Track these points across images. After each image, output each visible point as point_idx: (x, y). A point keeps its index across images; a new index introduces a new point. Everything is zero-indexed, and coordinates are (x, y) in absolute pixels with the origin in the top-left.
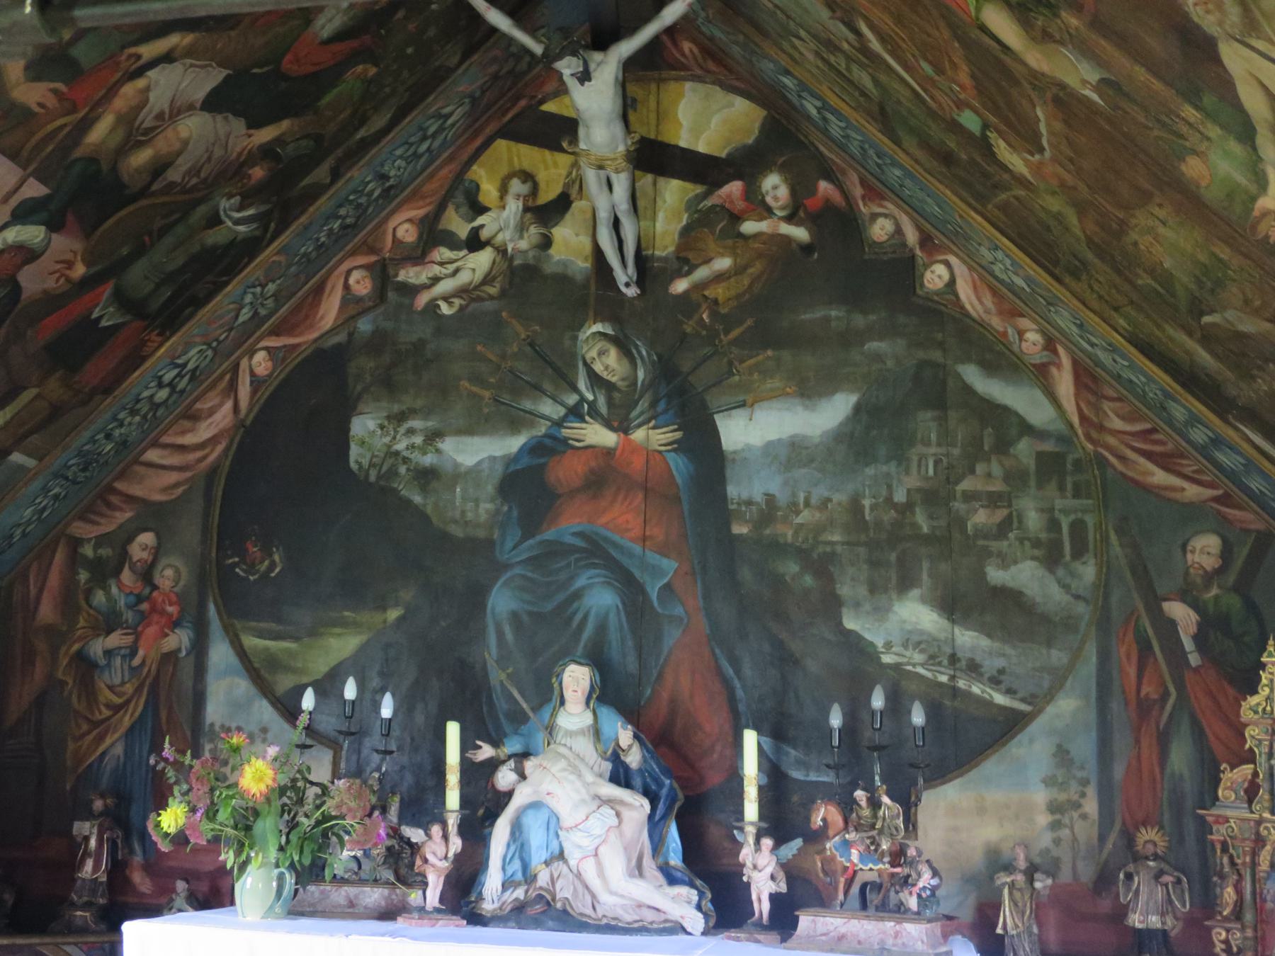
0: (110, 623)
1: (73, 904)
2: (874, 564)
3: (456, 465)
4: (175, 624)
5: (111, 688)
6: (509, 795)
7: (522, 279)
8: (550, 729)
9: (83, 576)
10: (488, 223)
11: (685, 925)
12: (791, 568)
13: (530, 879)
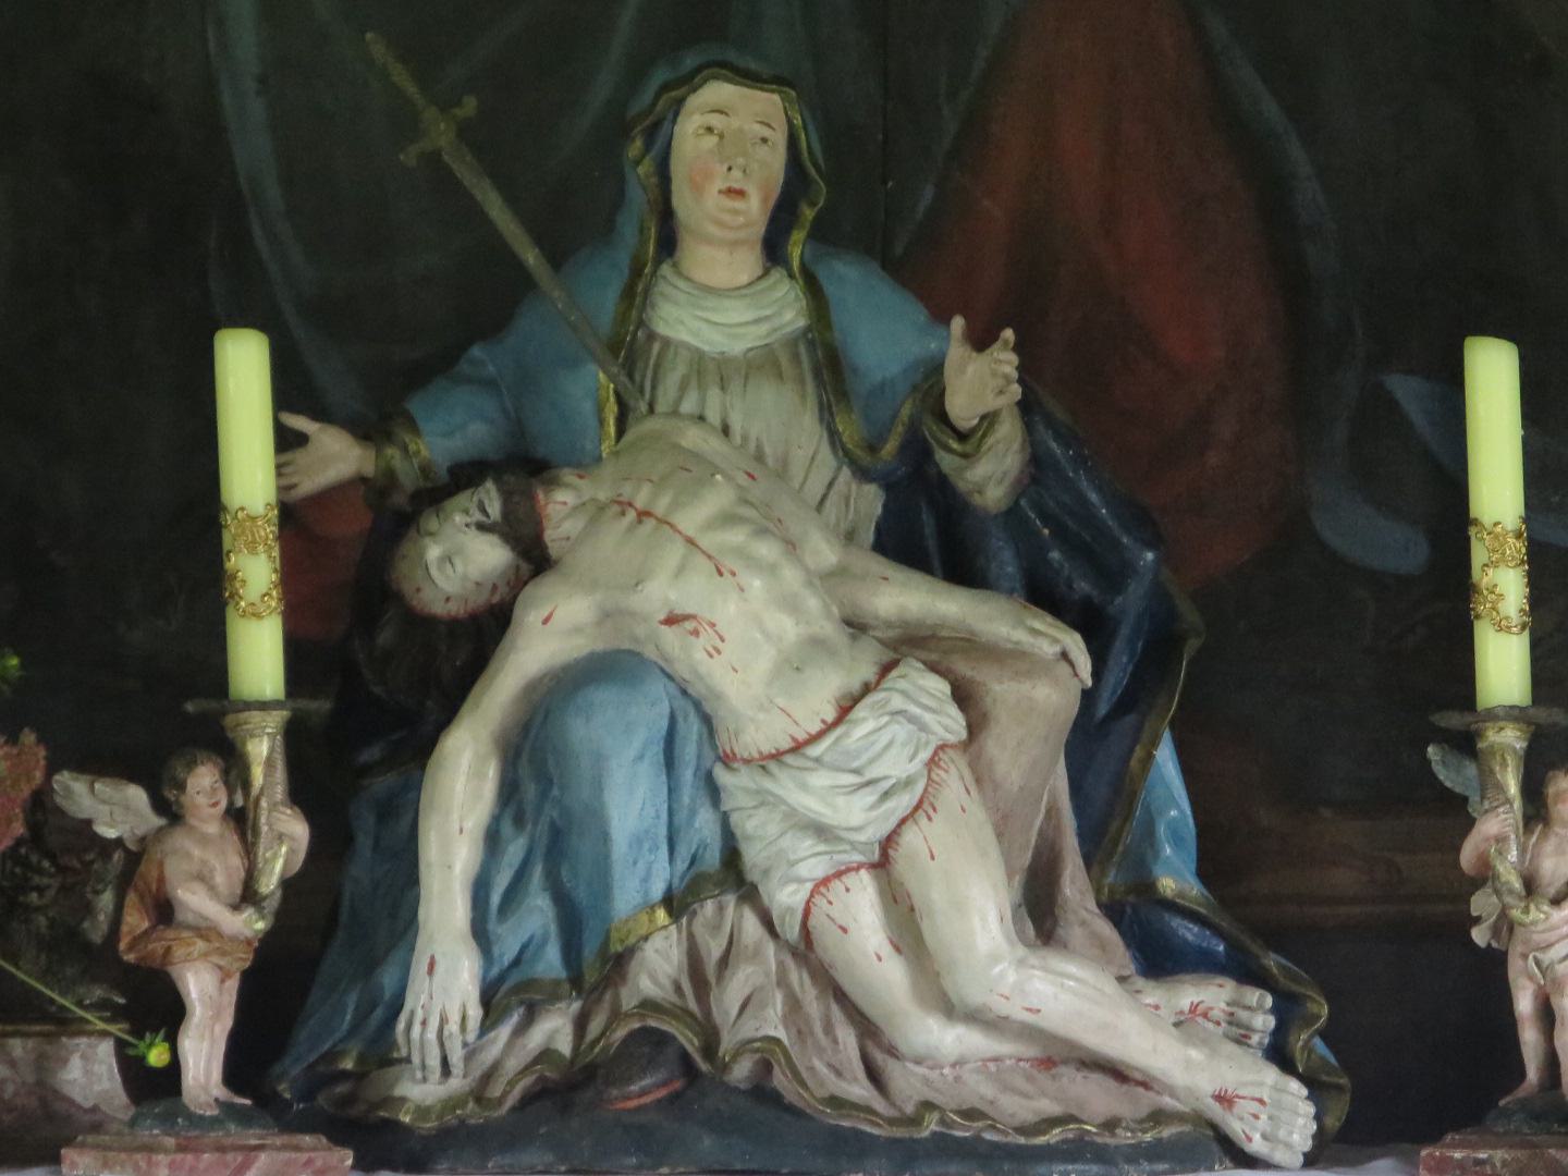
6: (487, 628)
8: (631, 350)
11: (1235, 1127)
13: (596, 964)
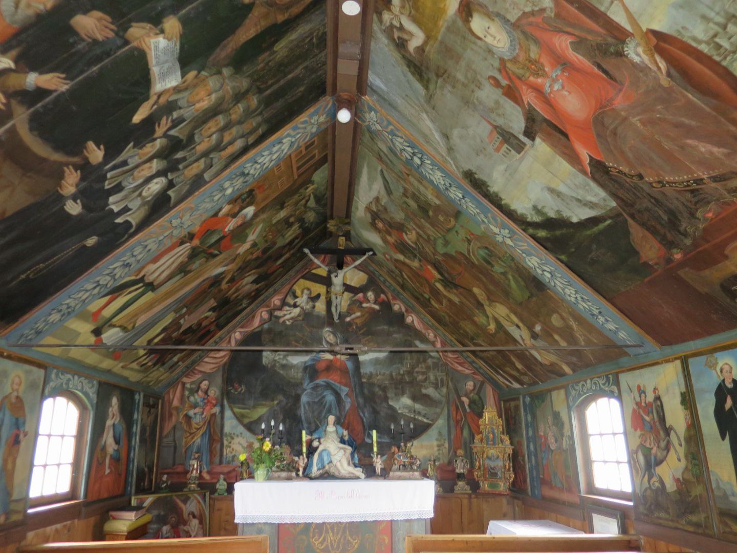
0: (195, 406)
1: (190, 483)
2: (396, 388)
3: (292, 364)
4: (215, 406)
5: (196, 424)
6: (317, 448)
7: (307, 316)
9: (187, 393)
10: (298, 301)
12: (377, 389)
13: (324, 467)
